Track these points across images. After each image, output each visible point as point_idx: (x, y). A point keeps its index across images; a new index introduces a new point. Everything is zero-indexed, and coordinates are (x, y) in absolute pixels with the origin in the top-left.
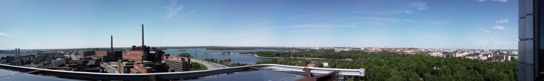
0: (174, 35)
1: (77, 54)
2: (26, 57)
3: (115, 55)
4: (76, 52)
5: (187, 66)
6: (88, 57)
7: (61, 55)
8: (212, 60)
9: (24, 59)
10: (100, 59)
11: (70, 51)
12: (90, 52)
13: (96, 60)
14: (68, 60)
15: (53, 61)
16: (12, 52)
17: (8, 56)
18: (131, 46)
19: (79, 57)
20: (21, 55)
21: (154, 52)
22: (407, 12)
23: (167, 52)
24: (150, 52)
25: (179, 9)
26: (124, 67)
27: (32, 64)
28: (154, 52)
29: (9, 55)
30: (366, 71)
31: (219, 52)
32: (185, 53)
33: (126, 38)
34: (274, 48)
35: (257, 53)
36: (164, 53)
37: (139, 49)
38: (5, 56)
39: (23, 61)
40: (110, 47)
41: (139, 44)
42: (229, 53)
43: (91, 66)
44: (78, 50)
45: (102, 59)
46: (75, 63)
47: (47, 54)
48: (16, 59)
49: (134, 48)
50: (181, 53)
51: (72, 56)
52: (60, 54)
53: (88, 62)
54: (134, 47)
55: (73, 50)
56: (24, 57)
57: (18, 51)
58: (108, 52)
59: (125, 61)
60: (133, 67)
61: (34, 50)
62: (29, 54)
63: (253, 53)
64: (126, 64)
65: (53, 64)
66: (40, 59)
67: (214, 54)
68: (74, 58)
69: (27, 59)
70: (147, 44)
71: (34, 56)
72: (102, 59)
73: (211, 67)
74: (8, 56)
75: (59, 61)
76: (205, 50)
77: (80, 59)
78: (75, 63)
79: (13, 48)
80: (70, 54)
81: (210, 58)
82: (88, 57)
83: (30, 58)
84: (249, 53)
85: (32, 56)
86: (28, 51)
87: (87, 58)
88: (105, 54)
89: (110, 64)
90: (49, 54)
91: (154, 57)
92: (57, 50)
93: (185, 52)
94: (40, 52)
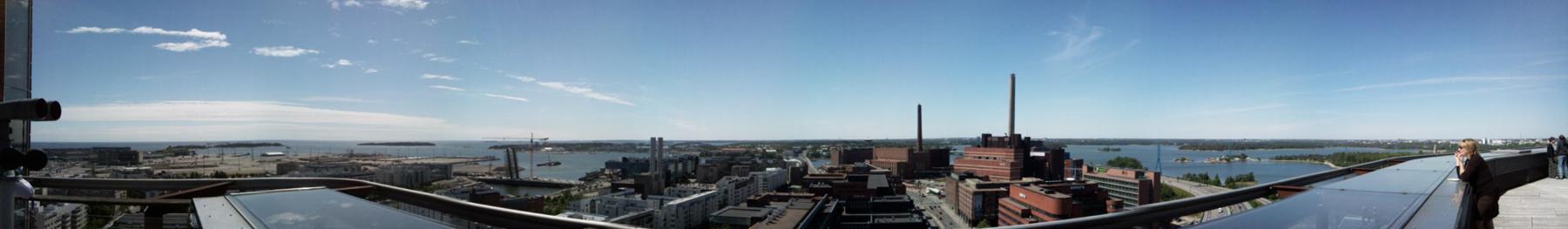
0: (1084, 106)
1: (815, 156)
3: (931, 159)
4: (815, 149)
5: (1151, 190)
7: (777, 160)
8: (1204, 179)
9: (672, 168)
11: (797, 147)
12: (857, 153)
14: (799, 175)
18: (975, 133)
19: (828, 164)
20: (665, 155)
21: (1042, 154)
23: (1074, 153)
24: (1033, 154)
25: (1093, 37)
26: (975, 194)
28: (1042, 154)
29: (627, 155)
31: (1217, 157)
32: (1120, 153)
33: (962, 113)
34: (1378, 144)
35: (1329, 158)
36: (1067, 156)
37: (1000, 143)
38: (618, 157)
40: (915, 136)
41: (1000, 130)
42: (1244, 157)
43: (881, 192)
44: (816, 144)
48: (652, 167)
49: (987, 141)
50: (1112, 156)
53: (866, 179)
54: (986, 136)
56: (670, 161)
57: (657, 144)
58: (910, 151)
59: (971, 175)
60: (1007, 194)
61: (688, 143)
63: (1321, 158)
64: (978, 186)
67: (1204, 161)
68: (814, 168)
69: (680, 166)
70: (1023, 130)
71: (697, 160)
73: (1200, 192)
75: (774, 177)
76: (1175, 149)
77: (831, 170)
81: (1197, 172)
84: (1496, 147)
85: (690, 158)
87: (856, 170)
88: (902, 156)
89: (919, 186)
90: (737, 154)
91: (1042, 162)
92: (754, 144)
93: (1122, 154)
94: (706, 148)
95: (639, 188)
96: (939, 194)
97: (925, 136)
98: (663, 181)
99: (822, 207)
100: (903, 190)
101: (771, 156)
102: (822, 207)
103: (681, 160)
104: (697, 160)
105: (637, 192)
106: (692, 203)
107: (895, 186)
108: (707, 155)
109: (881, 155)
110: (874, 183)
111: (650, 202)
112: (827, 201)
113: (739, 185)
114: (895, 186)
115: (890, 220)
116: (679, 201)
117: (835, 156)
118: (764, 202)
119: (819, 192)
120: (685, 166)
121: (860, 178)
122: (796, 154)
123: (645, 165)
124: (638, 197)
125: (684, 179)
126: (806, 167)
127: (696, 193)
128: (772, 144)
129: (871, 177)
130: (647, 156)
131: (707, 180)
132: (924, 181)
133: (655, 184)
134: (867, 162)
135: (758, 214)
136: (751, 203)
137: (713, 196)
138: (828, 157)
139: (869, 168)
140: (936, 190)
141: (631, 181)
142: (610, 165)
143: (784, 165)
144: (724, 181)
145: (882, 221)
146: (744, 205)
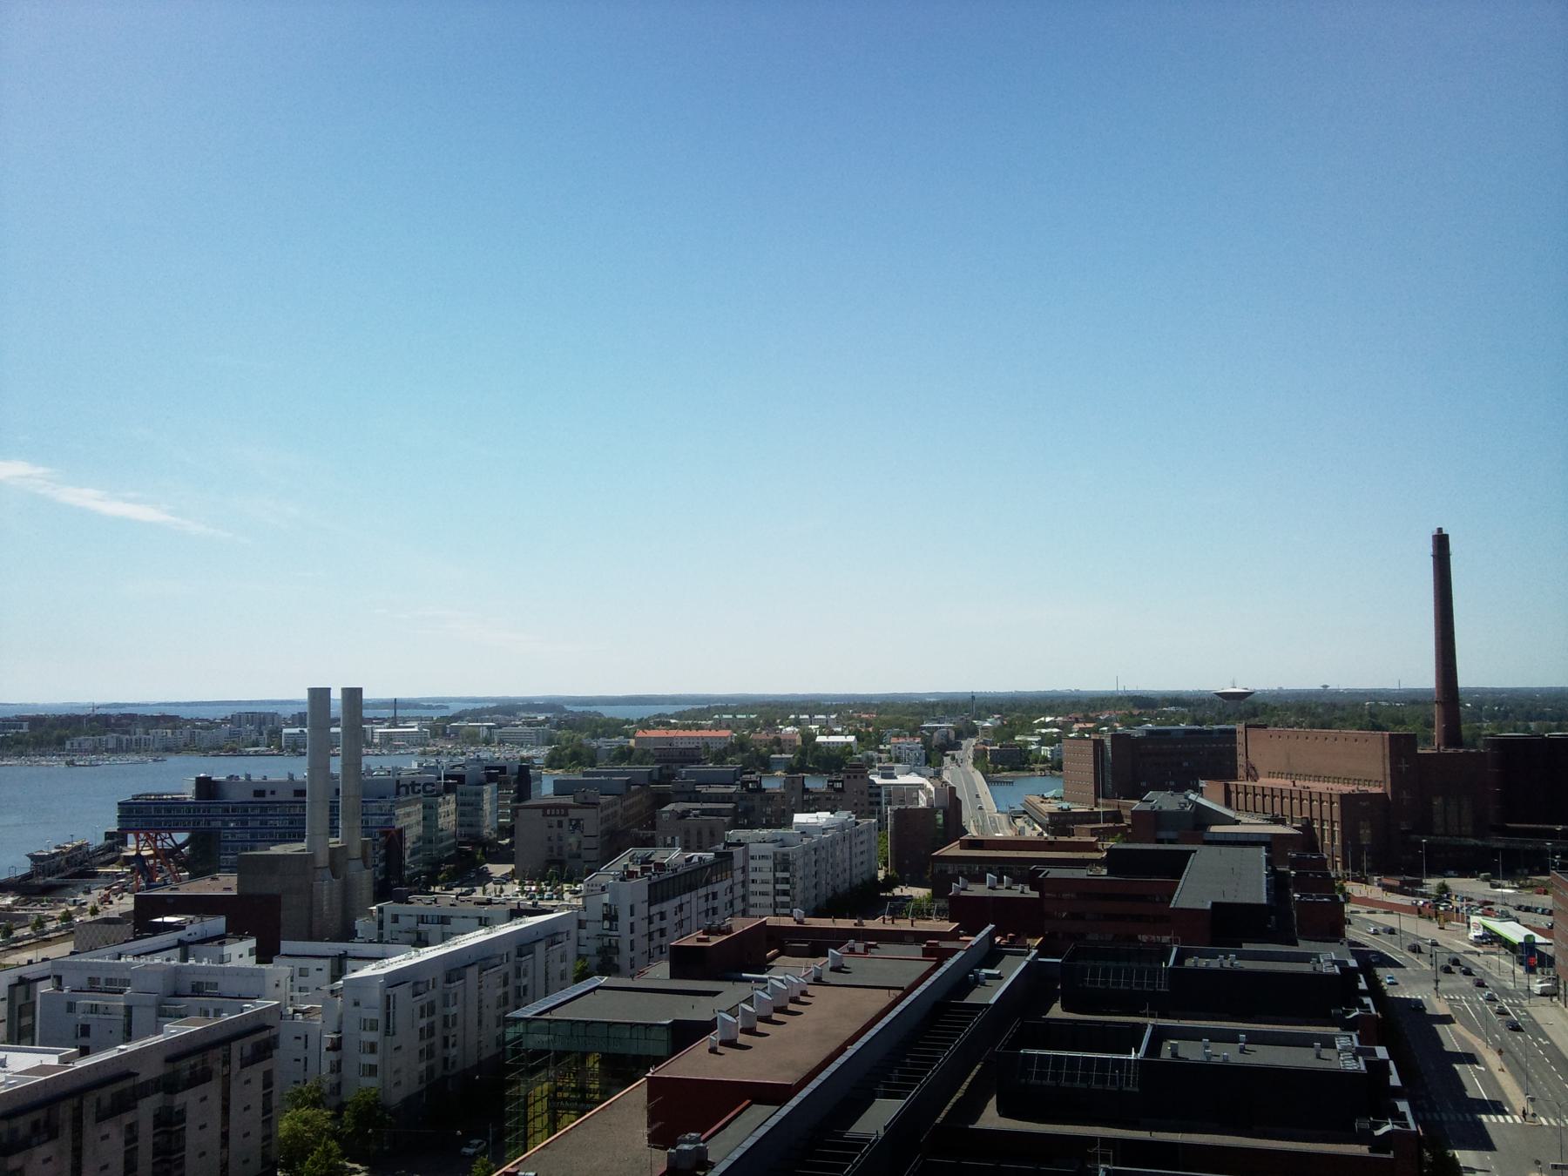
1: (1007, 761)
2: (425, 791)
4: (1005, 731)
6: (1163, 800)
7: (841, 777)
9: (410, 819)
10: (1308, 838)
11: (935, 726)
12: (1168, 749)
13: (1273, 844)
14: (924, 838)
15: (758, 840)
16: (253, 727)
17: (206, 787)
19: (1048, 795)
20: (377, 764)
22: (1048, 719)
27: (504, 884)
29: (220, 769)
30: (1396, 1088)
38: (176, 778)
39: (393, 840)
40: (1424, 678)
43: (1229, 923)
44: (1018, 711)
45: (1331, 841)
46: (1002, 868)
47: (674, 758)
48: (315, 817)
51: (946, 776)
52: (813, 758)
53: (1175, 865)
55: (963, 713)
56: (403, 788)
57: (338, 720)
58: (1401, 747)
61: (506, 710)
62: (451, 757)
65: (763, 872)
66: (592, 821)
68: (992, 811)
69: (448, 813)
71: (522, 779)
72: (1331, 841)
74: (206, 787)
75: (821, 848)
77: (1061, 823)
78: (1002, 868)
79: (278, 682)
80: (933, 755)
82: (1163, 800)
83: (468, 810)
85: (495, 774)
86: (446, 724)
87: (1153, 822)
88: (1365, 768)
89: (1438, 909)
90: (690, 756)
92: (774, 710)
94: (576, 730)
95: (259, 919)
96: (1528, 955)
97: (1468, 677)
98: (364, 879)
99: (964, 982)
100: (1331, 925)
101: (832, 761)
102: (964, 982)
103: (455, 782)
104: (522, 779)
105: (236, 930)
106: (454, 968)
107: (1301, 893)
108: (578, 757)
109: (1269, 761)
110: (1214, 879)
111: (279, 969)
112: (992, 956)
113: (665, 887)
114: (1301, 893)
115: (1228, 1053)
116: (403, 960)
117: (1082, 766)
118: (744, 956)
119: (969, 914)
120: (468, 810)
121: (1151, 864)
122: (933, 755)
123: (276, 811)
124: (240, 953)
125: (464, 862)
126: (952, 805)
127: (492, 919)
128: (845, 710)
129: (1203, 859)
130: (299, 768)
131: (557, 869)
132: (1461, 885)
133: (326, 890)
134: (1209, 797)
135: (699, 1010)
136: (687, 963)
137: (550, 935)
138: (1056, 766)
139: (1203, 818)
140: (1515, 932)
141: (224, 884)
142: (141, 814)
143: (871, 800)
144: (608, 875)
145: (1192, 1052)
146: (660, 972)
